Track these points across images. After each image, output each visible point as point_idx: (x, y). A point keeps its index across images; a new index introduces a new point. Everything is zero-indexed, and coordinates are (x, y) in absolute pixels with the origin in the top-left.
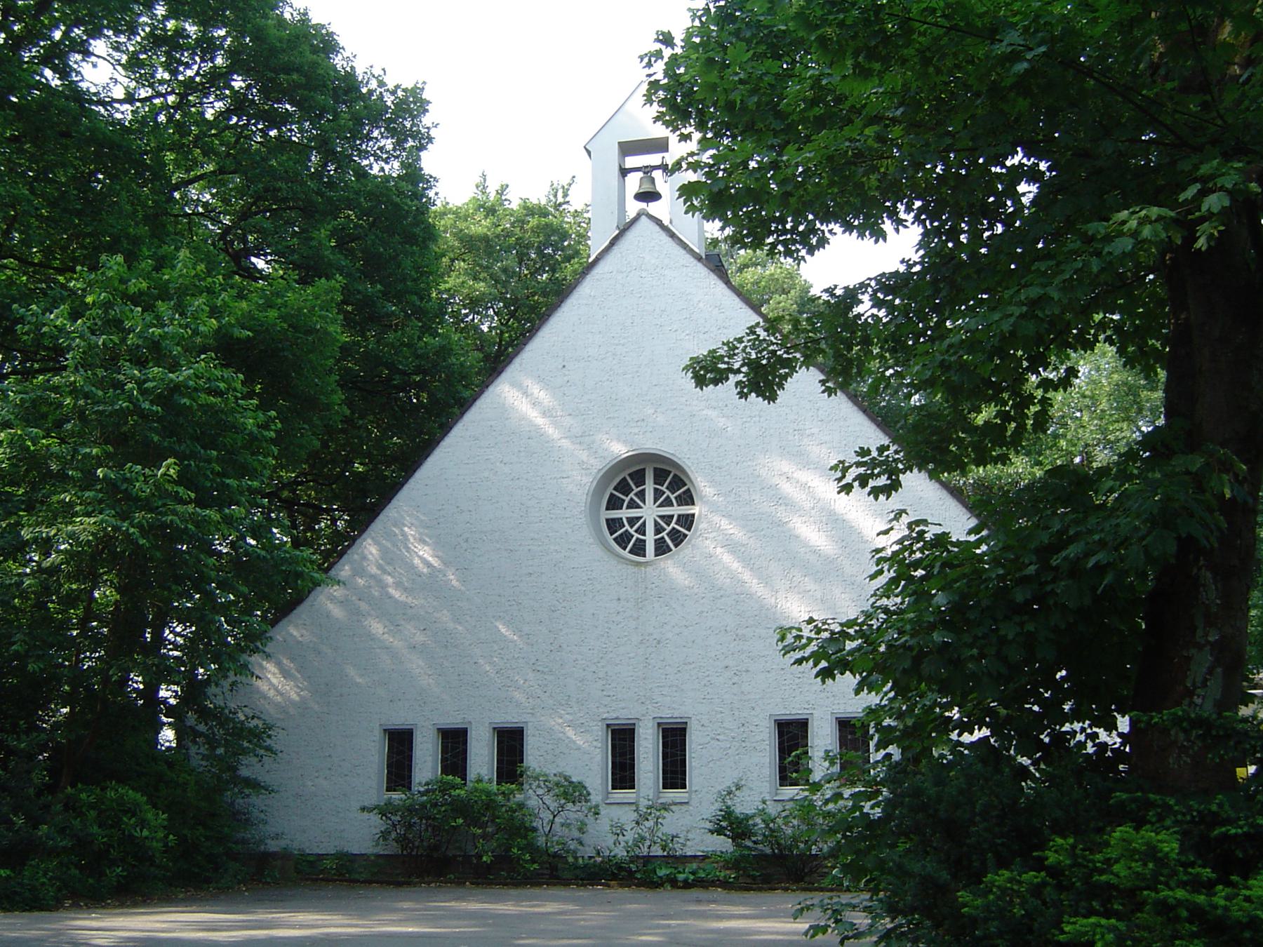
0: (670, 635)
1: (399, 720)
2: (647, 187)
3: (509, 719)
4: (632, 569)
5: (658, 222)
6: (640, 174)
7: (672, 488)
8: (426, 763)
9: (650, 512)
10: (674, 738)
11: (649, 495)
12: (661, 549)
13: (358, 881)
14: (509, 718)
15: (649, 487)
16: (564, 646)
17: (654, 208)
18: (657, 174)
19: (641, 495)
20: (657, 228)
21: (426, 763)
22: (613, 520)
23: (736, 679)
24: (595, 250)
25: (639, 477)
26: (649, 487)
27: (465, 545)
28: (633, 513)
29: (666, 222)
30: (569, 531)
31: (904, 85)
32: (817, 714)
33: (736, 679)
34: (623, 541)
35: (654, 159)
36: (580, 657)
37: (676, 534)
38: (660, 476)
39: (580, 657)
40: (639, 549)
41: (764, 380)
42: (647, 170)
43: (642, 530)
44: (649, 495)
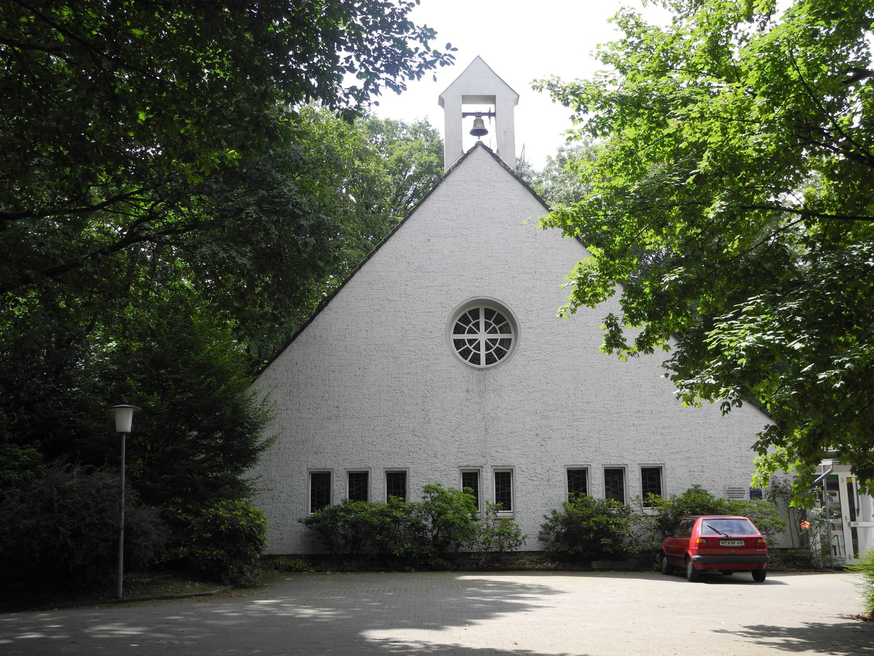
0: (500, 415)
1: (321, 464)
2: (479, 127)
3: (396, 465)
4: (476, 372)
5: (489, 151)
6: (474, 118)
7: (497, 322)
8: (340, 491)
9: (482, 336)
10: (504, 479)
11: (482, 326)
12: (490, 360)
13: (211, 595)
14: (397, 464)
15: (482, 321)
16: (433, 420)
17: (484, 139)
18: (485, 118)
19: (477, 325)
20: (489, 155)
21: (340, 491)
22: (459, 340)
23: (543, 443)
24: (446, 170)
25: (475, 314)
26: (482, 321)
27: (364, 353)
28: (472, 336)
29: (495, 151)
30: (434, 347)
31: (675, 370)
32: (593, 465)
33: (543, 443)
34: (465, 354)
35: (484, 108)
36: (443, 427)
37: (498, 352)
38: (489, 314)
39: (443, 427)
40: (476, 360)
41: (609, 325)
42: (479, 115)
43: (478, 347)
44: (482, 326)
